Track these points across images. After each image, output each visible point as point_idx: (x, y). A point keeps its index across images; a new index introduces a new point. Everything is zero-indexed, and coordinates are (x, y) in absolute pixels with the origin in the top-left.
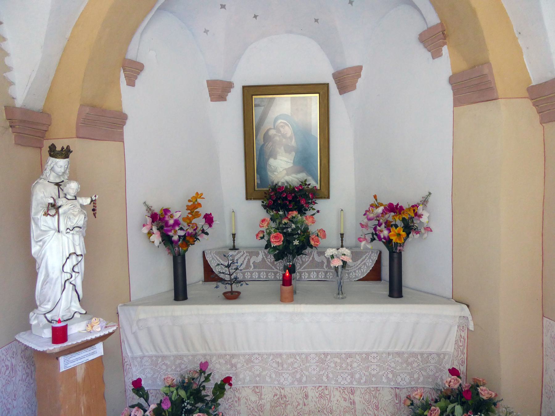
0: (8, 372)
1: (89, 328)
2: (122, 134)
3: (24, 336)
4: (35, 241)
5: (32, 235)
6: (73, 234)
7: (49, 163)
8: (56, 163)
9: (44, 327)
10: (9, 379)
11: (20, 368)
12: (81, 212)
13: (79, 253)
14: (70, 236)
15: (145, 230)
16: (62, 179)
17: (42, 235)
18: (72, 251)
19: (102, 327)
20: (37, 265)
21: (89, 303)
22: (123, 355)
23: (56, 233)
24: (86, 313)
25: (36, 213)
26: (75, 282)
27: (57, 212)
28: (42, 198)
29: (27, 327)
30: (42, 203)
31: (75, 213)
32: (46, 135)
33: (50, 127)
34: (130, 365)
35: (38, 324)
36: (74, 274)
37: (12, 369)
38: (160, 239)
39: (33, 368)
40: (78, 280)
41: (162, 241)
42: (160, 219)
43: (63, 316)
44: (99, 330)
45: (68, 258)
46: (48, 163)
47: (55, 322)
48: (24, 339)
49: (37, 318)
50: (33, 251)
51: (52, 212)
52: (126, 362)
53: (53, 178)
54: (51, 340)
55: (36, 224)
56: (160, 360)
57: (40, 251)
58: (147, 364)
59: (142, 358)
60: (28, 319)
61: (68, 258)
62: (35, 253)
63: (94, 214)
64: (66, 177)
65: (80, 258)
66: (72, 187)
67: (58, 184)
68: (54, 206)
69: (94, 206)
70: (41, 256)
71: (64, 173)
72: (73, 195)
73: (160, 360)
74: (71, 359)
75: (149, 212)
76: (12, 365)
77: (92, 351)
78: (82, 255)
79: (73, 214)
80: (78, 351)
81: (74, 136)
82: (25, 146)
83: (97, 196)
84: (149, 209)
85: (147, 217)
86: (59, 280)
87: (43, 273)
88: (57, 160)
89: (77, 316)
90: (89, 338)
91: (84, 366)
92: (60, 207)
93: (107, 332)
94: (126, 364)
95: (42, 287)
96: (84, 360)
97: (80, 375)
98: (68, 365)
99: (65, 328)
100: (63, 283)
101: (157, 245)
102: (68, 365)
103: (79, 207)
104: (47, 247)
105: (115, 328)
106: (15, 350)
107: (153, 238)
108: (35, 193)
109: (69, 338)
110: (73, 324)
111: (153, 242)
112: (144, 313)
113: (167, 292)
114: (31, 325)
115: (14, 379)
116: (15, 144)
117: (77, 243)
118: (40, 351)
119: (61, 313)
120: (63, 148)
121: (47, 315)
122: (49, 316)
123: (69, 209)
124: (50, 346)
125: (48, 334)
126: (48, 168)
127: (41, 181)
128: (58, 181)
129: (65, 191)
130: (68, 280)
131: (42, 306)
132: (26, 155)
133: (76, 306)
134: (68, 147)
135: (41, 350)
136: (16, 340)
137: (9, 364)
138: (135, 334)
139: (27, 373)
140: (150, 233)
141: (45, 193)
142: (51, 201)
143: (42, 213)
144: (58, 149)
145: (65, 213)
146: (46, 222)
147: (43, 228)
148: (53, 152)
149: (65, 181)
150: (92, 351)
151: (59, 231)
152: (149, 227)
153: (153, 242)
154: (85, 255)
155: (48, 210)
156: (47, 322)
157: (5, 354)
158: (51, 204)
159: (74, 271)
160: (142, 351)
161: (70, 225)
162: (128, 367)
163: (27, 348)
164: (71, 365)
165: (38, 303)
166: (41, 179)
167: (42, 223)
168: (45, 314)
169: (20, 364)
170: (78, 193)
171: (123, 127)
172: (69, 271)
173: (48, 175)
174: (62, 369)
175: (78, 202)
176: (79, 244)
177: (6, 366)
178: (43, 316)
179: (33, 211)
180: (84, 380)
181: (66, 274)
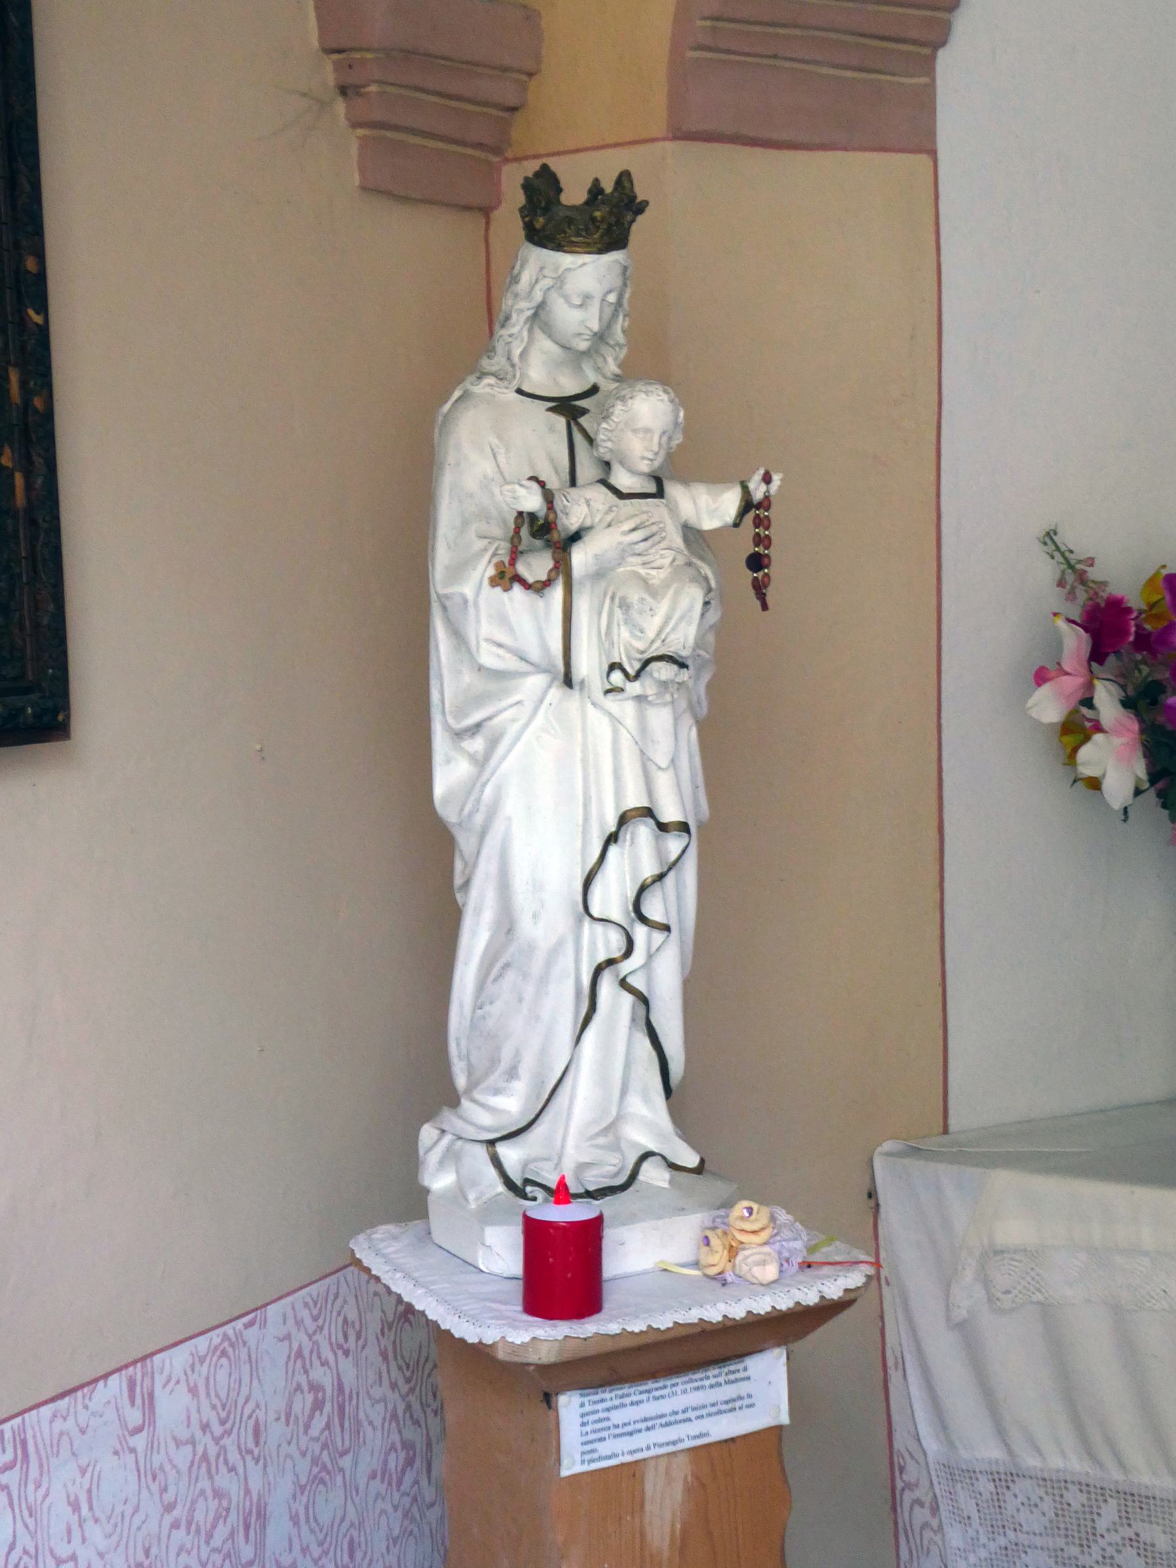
0: (319, 1423)
1: (717, 1259)
2: (924, 103)
3: (391, 1248)
4: (447, 727)
5: (435, 696)
6: (640, 699)
7: (526, 278)
8: (560, 281)
9: (489, 1214)
10: (325, 1456)
11: (377, 1414)
12: (686, 570)
13: (670, 813)
14: (625, 709)
15: (1048, 706)
16: (592, 378)
17: (480, 700)
18: (635, 799)
19: (784, 1262)
20: (458, 865)
21: (711, 1102)
22: (898, 1444)
23: (556, 693)
24: (699, 1170)
25: (458, 571)
26: (649, 981)
27: (562, 567)
28: (486, 484)
29: (411, 1205)
30: (484, 515)
31: (657, 577)
32: (515, 134)
33: (533, 83)
34: (935, 1510)
35: (459, 1194)
36: (640, 933)
37: (342, 1408)
38: (1140, 769)
39: (434, 1423)
40: (664, 971)
41: (1154, 778)
42: (1143, 641)
43: (582, 1167)
44: (766, 1282)
45: (612, 838)
46: (515, 280)
47: (540, 1194)
48: (387, 1255)
49: (451, 1157)
50: (439, 789)
51: (537, 566)
52: (909, 1486)
53: (544, 371)
54: (517, 1288)
55: (458, 635)
56: (1109, 1512)
57: (474, 785)
58: (1033, 1521)
59: (1005, 1478)
60: (411, 1161)
61: (612, 838)
62: (446, 801)
63: (759, 589)
64: (612, 367)
65: (674, 845)
66: (644, 420)
67: (568, 408)
68: (545, 534)
69: (758, 540)
70: (479, 819)
71: (601, 337)
72: (645, 467)
73: (1109, 1512)
74: (618, 1417)
75: (1071, 596)
76: (341, 1388)
77: (728, 1392)
78: (684, 827)
79: (645, 582)
80: (654, 1375)
81: (659, 127)
82: (405, 199)
83: (777, 479)
84: (1075, 573)
85: (1061, 623)
86: (566, 961)
87: (488, 915)
88: (566, 260)
89: (654, 1175)
90: (714, 1314)
91: (682, 1470)
92: (576, 537)
93: (810, 1298)
94: (908, 1497)
95: (481, 987)
96: (687, 1435)
97: (664, 1510)
98: (604, 1448)
99: (589, 1235)
100: (586, 981)
101: (1117, 804)
102: (604, 1448)
103: (678, 542)
104: (508, 764)
105: (855, 1279)
106: (352, 1315)
107: (1095, 756)
108: (451, 458)
109: (612, 1297)
110: (631, 1219)
111: (1095, 784)
112: (1023, 1213)
113: (1160, 1103)
114: (426, 1191)
115: (346, 1462)
116: (364, 188)
117: (661, 756)
118: (462, 1341)
119: (569, 1147)
120: (596, 190)
121: (502, 1149)
122: (510, 1154)
123: (625, 552)
124: (514, 1325)
125: (502, 1254)
126: (519, 310)
127: (483, 387)
128: (569, 386)
129: (604, 449)
130: (610, 962)
131: (477, 1095)
132: (413, 243)
133: (648, 1123)
134: (624, 180)
135: (518, 1342)
136: (358, 1263)
137: (327, 1380)
138: (966, 1333)
139: (408, 1446)
140: (1077, 728)
141: (502, 459)
142: (532, 501)
143: (485, 569)
144: (574, 195)
145: (599, 574)
146: (503, 620)
147: (489, 657)
148: (553, 220)
149: (606, 386)
150: (728, 1392)
151: (568, 681)
152: (1072, 684)
153: (1095, 784)
154: (701, 826)
155: (515, 554)
156: (501, 1188)
157: (310, 1325)
158: (532, 516)
159: (643, 919)
160: (1001, 1433)
161: (629, 644)
162: (921, 1515)
163: (408, 1313)
164: (618, 1451)
165: (461, 1081)
166: (483, 375)
167: (490, 626)
168: (492, 1143)
169: (377, 1392)
170: (670, 456)
171: (933, 58)
172: (616, 915)
173: (516, 352)
174: (572, 1464)
175: (673, 510)
176: (673, 762)
177: (315, 1388)
178: (481, 1152)
179: (442, 556)
180: (682, 1544)
181: (599, 928)
